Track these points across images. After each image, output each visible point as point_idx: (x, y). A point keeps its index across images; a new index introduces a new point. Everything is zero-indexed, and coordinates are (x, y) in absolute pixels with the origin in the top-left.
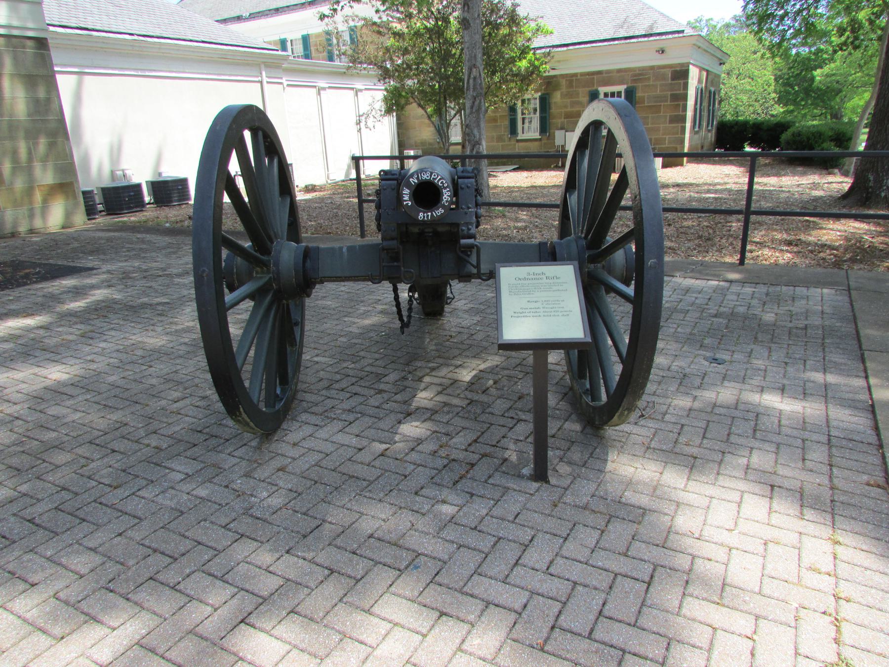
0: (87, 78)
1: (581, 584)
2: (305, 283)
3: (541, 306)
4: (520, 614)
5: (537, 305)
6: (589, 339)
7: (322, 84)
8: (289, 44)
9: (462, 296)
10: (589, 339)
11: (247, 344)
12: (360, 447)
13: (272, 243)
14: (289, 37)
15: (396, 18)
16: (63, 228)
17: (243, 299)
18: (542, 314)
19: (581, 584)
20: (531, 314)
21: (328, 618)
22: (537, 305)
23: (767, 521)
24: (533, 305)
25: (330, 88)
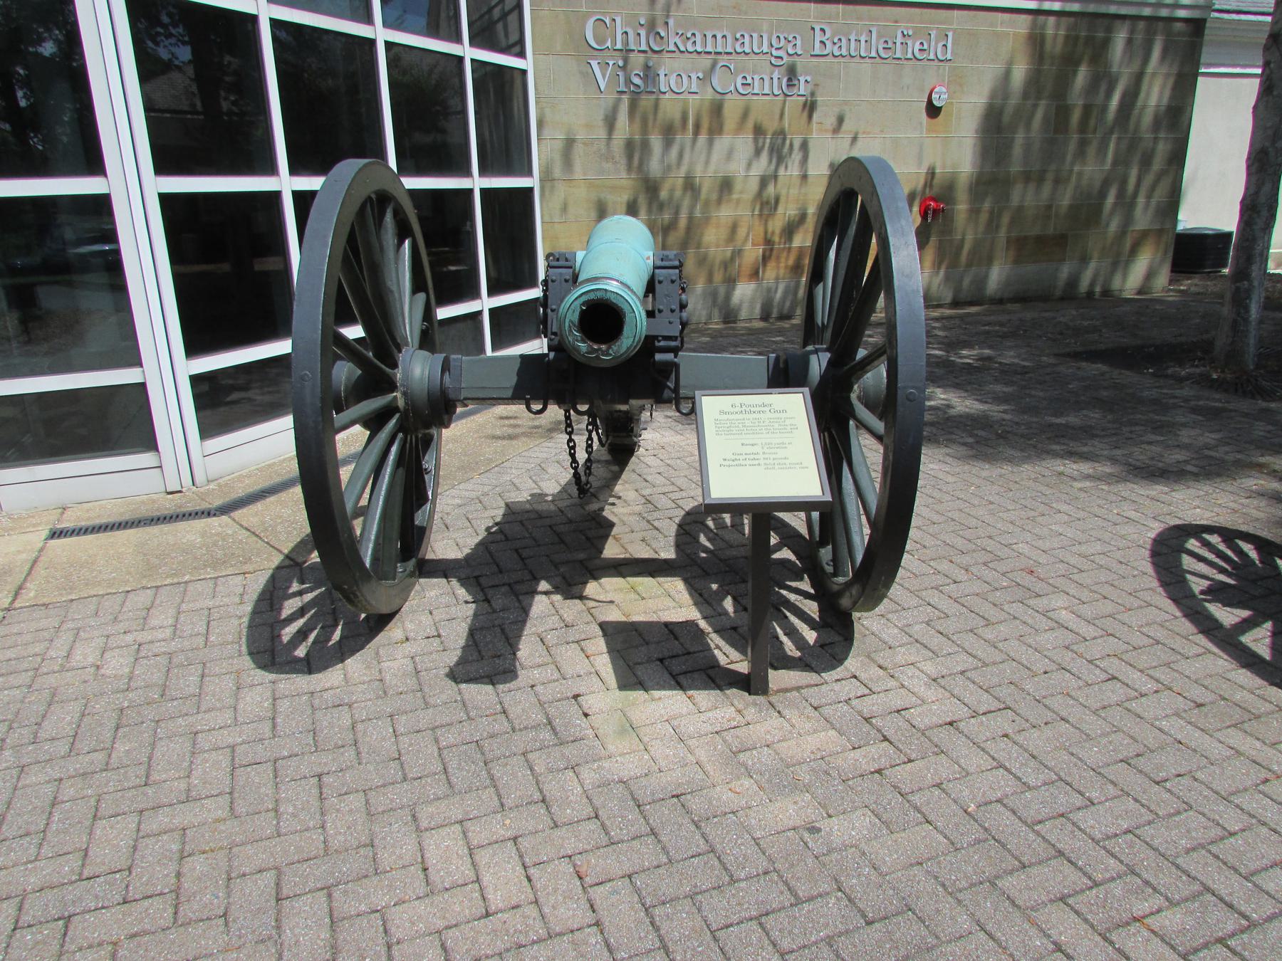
1: (76, 881)
2: (440, 408)
3: (760, 451)
4: (691, 896)
5: (755, 450)
6: (828, 498)
9: (658, 433)
10: (828, 498)
11: (359, 486)
12: (1199, 701)
13: (400, 351)
15: (1188, 378)
16: (1139, 293)
17: (352, 423)
18: (762, 462)
19: (76, 881)
20: (748, 462)
21: (181, 913)
22: (755, 450)
23: (556, 741)
24: (749, 449)
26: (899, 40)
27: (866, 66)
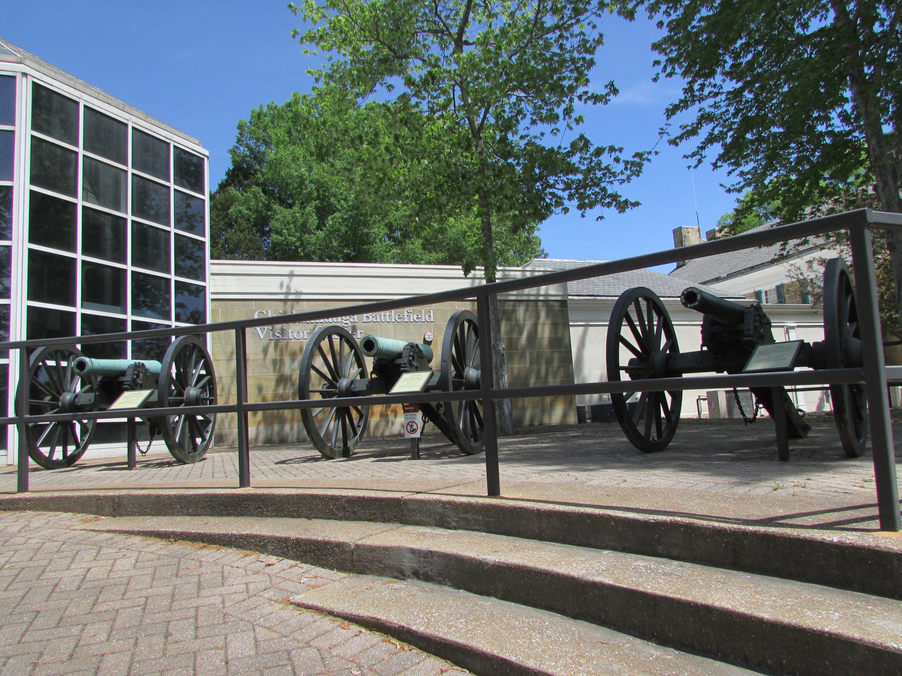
0: (590, 328)
7: (790, 324)
8: (763, 295)
14: (763, 289)
25: (799, 326)
26: (406, 314)
27: (391, 326)
